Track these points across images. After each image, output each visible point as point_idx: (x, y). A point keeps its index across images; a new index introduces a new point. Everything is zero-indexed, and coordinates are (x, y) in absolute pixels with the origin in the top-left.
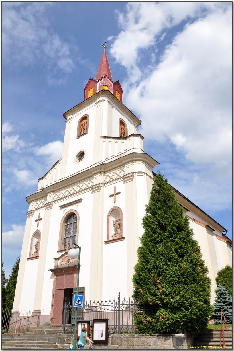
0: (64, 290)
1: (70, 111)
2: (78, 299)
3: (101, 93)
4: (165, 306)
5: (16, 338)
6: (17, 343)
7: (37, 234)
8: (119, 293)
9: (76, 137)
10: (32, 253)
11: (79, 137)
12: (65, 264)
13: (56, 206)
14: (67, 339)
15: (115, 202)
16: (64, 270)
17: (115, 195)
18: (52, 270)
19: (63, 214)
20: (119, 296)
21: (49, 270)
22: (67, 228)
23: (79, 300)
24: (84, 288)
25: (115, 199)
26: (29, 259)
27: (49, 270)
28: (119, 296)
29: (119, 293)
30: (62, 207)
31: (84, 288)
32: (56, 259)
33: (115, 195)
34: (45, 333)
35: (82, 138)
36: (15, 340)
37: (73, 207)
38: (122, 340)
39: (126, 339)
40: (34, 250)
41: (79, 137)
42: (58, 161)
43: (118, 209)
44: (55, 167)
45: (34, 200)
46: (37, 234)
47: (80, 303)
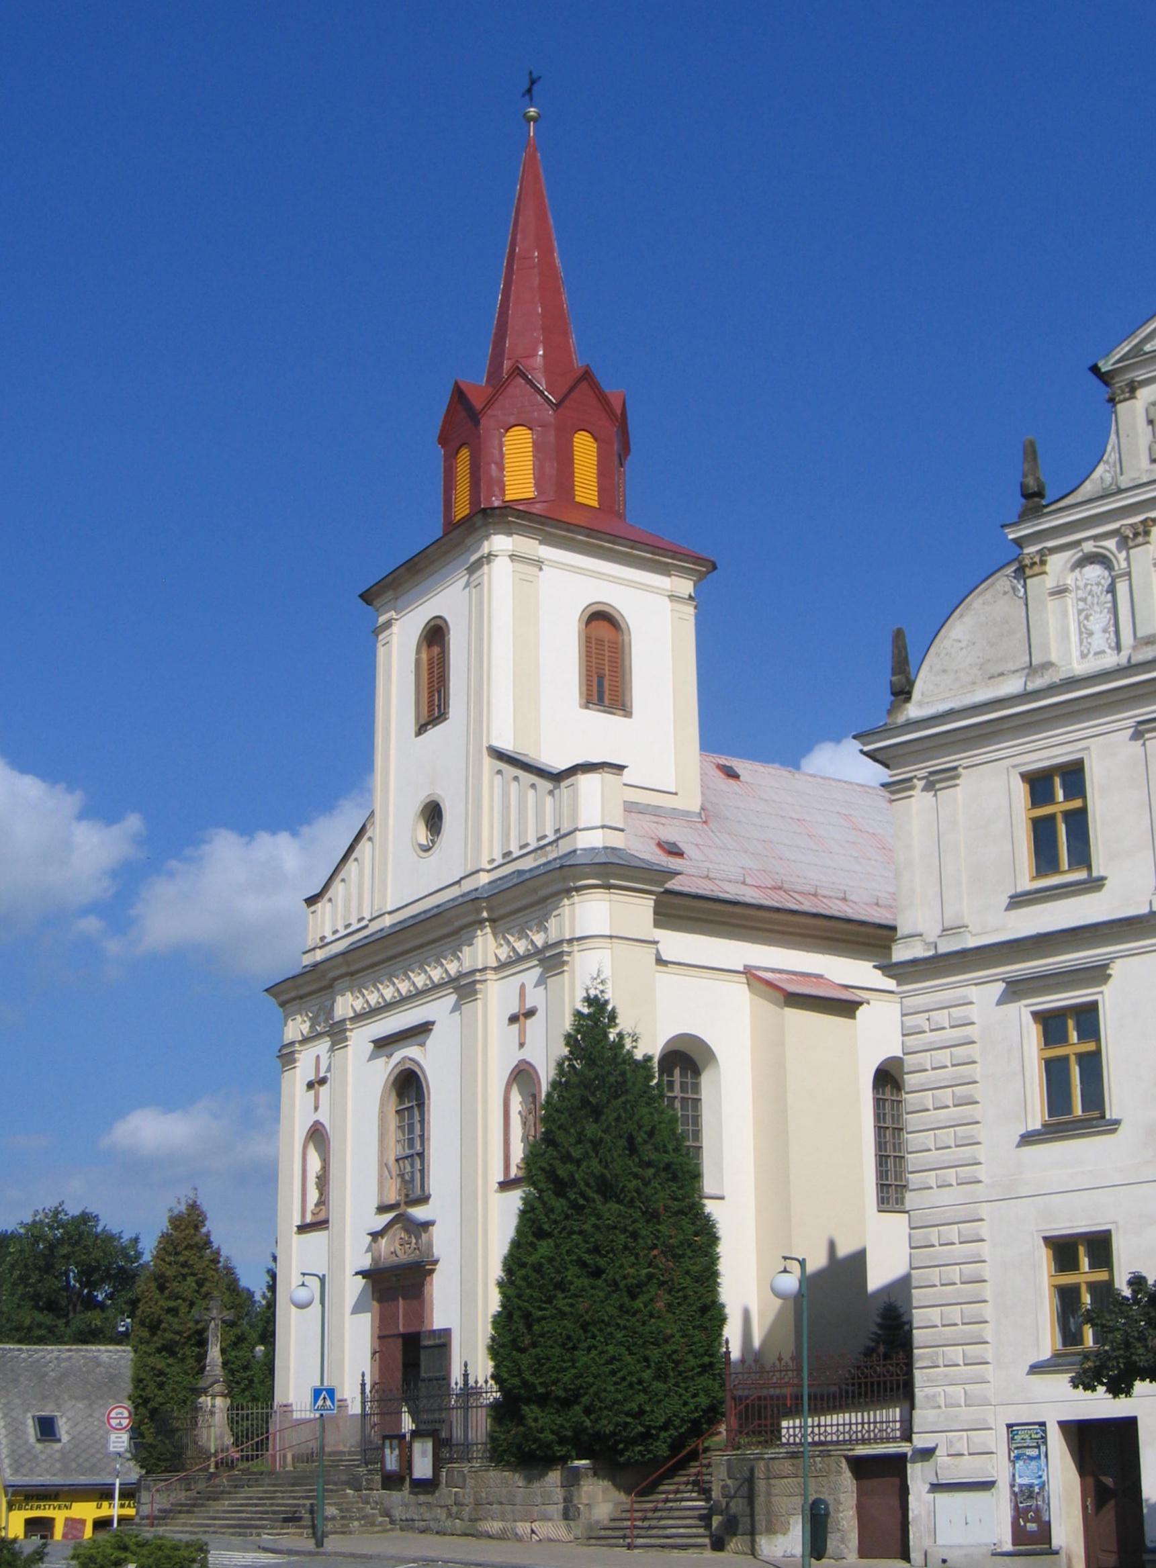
0: (400, 1341)
1: (381, 584)
2: (322, 1396)
3: (478, 519)
4: (542, 1401)
5: (267, 1481)
6: (265, 1492)
7: (317, 1135)
8: (466, 1365)
9: (411, 727)
10: (311, 1206)
11: (421, 729)
12: (399, 1253)
13: (361, 1038)
14: (367, 1480)
15: (522, 1045)
16: (396, 1275)
17: (522, 1018)
18: (364, 1274)
19: (383, 1070)
20: (466, 1371)
21: (357, 1273)
22: (404, 1121)
23: (324, 1398)
24: (447, 1332)
25: (522, 1033)
26: (303, 1229)
27: (357, 1273)
28: (466, 1371)
29: (466, 1365)
30: (383, 1044)
31: (447, 1332)
32: (376, 1235)
33: (522, 1018)
34: (338, 1466)
35: (433, 733)
36: (262, 1486)
37: (411, 1051)
38: (464, 1476)
39: (473, 1474)
40: (313, 1195)
41: (421, 729)
42: (362, 831)
43: (531, 1071)
44: (354, 856)
45: (293, 999)
46: (317, 1135)
47: (328, 1403)
